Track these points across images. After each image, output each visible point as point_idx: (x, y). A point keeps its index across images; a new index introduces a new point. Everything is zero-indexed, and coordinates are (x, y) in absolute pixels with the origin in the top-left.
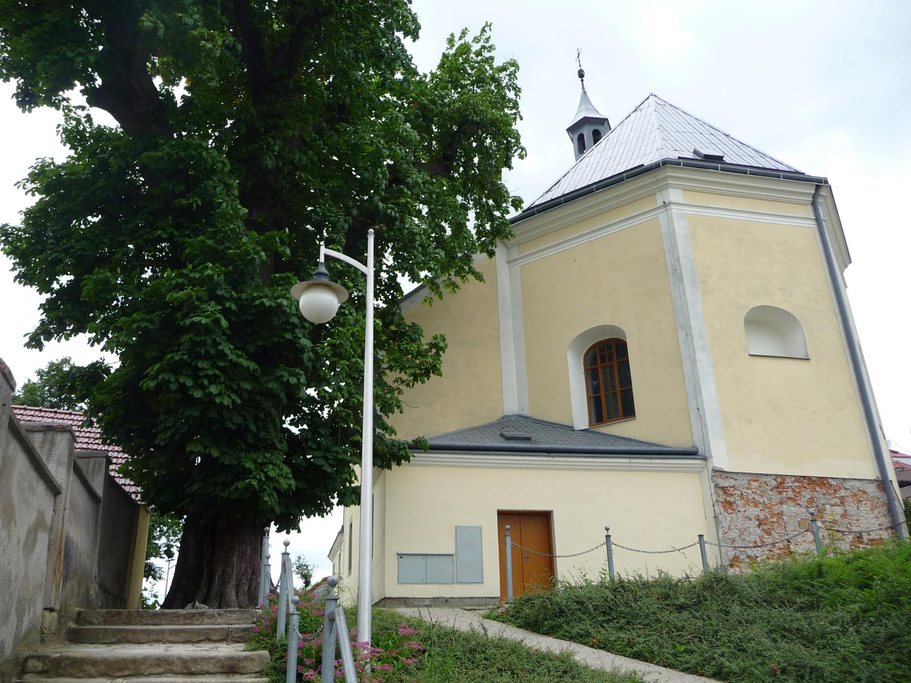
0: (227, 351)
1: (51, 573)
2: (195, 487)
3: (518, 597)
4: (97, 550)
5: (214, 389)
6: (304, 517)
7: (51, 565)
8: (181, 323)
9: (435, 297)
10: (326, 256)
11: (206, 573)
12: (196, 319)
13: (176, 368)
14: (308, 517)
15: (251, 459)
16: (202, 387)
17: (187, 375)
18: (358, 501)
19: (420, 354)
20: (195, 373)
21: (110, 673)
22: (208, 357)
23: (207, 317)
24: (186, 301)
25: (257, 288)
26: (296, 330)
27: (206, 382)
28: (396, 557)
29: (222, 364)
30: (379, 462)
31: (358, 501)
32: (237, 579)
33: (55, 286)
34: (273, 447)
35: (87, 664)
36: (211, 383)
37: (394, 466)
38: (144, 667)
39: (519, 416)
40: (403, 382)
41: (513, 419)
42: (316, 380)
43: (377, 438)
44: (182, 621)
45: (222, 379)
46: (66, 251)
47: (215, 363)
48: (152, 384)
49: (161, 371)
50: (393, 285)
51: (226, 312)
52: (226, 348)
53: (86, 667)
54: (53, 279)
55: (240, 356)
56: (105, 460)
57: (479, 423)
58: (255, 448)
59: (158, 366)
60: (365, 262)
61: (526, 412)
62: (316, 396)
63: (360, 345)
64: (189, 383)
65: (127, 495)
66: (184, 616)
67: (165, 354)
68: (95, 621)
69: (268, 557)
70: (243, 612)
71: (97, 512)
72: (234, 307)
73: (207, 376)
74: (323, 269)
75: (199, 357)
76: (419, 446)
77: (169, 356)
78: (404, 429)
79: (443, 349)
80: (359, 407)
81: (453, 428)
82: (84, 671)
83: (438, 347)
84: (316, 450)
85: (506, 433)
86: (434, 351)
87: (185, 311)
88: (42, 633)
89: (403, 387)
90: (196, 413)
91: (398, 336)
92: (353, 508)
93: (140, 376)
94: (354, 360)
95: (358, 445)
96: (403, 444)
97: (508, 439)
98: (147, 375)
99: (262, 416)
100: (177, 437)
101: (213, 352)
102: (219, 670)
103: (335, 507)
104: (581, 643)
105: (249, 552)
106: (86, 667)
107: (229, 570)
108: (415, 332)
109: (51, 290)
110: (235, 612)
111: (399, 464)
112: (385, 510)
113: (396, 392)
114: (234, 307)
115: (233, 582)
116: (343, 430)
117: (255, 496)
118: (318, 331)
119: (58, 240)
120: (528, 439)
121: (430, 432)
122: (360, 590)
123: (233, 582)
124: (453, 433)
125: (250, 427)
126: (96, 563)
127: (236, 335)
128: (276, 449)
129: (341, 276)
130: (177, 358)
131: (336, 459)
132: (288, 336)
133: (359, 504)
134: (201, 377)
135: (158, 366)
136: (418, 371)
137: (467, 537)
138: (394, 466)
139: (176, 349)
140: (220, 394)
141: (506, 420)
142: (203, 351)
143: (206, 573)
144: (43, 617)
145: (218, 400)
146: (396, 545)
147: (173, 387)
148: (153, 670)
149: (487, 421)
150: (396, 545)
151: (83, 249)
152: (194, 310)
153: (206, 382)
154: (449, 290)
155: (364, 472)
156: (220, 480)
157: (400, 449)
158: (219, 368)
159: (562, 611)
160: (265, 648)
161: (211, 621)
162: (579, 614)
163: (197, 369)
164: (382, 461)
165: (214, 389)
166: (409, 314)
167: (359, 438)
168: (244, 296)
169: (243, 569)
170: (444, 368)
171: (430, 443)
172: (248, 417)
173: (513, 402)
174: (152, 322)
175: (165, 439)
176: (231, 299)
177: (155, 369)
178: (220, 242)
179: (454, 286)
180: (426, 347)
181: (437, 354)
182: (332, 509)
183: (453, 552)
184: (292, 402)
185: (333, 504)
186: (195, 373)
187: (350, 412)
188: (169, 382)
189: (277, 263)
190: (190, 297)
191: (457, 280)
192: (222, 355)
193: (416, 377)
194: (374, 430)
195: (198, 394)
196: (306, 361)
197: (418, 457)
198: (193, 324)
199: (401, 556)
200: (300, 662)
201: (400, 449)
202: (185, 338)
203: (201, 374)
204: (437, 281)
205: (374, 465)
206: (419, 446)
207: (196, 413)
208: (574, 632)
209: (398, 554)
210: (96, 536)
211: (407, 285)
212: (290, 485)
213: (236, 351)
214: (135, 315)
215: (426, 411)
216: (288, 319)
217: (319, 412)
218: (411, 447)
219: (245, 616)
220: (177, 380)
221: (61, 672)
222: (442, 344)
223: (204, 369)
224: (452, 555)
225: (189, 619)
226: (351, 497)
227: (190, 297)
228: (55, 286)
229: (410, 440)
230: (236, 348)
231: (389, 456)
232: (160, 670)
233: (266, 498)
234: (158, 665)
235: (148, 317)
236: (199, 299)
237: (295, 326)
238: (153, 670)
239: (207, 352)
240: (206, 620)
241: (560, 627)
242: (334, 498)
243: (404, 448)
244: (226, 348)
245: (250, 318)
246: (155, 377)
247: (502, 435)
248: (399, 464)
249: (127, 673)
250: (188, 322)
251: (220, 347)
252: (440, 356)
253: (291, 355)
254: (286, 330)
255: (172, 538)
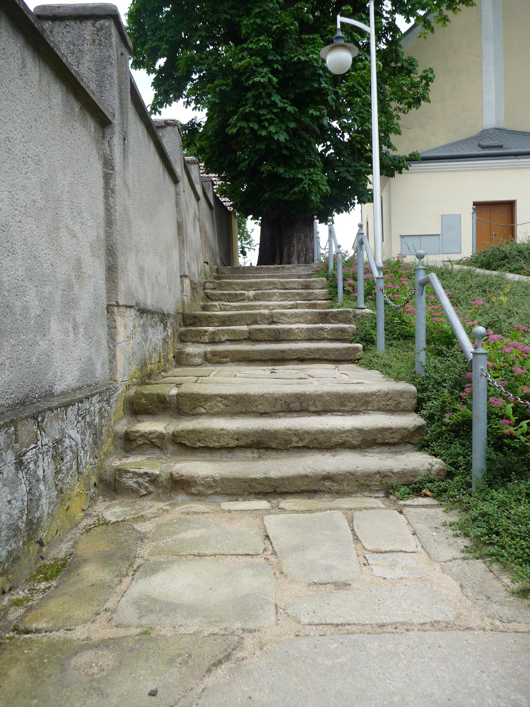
0: (277, 101)
1: (203, 244)
2: (267, 195)
3: (479, 251)
4: (216, 238)
5: (272, 129)
6: (335, 214)
7: (203, 239)
8: (247, 84)
9: (429, 32)
10: (342, 24)
11: (278, 251)
12: (257, 79)
13: (246, 117)
14: (339, 214)
15: (301, 173)
16: (264, 128)
17: (254, 121)
18: (371, 200)
19: (414, 85)
20: (259, 120)
21: (246, 289)
22: (265, 106)
23: (263, 77)
24: (247, 67)
25: (291, 50)
26: (321, 79)
27: (267, 124)
28: (400, 238)
29: (275, 111)
30: (385, 172)
31: (371, 200)
32: (297, 254)
33: (157, 67)
34: (315, 166)
35: (234, 284)
36: (270, 125)
37: (396, 173)
38: (262, 286)
39: (496, 129)
40: (400, 110)
41: (491, 132)
42: (336, 115)
43: (382, 155)
44: (272, 272)
45: (277, 121)
46: (161, 39)
47: (271, 110)
48: (234, 130)
49: (238, 120)
50: (393, 27)
51: (274, 72)
52: (276, 98)
53: (234, 286)
54: (155, 64)
55: (285, 103)
56: (211, 183)
57: (463, 137)
58: (301, 166)
59: (235, 117)
60: (367, 21)
61: (502, 125)
62: (338, 127)
63: (368, 84)
64: (256, 127)
65: (225, 208)
66: (273, 268)
67: (238, 108)
68: (226, 273)
69: (318, 233)
70: (306, 266)
71: (213, 216)
72: (280, 68)
73: (266, 120)
74: (340, 34)
75: (260, 107)
76: (414, 158)
77: (241, 109)
78: (402, 147)
79: (431, 80)
80: (368, 134)
81: (442, 143)
82: (233, 288)
83: (427, 79)
84: (341, 166)
85: (482, 143)
86: (424, 82)
87: (248, 75)
88: (206, 275)
89: (401, 114)
90: (263, 147)
91: (395, 72)
92: (368, 204)
93: (224, 125)
94: (364, 96)
95: (370, 160)
96: (402, 158)
97: (483, 147)
98: (229, 125)
99: (305, 144)
100: (252, 164)
101: (268, 102)
102: (300, 287)
103: (356, 205)
104: (517, 273)
105: (303, 237)
106: (234, 286)
107: (292, 249)
108: (407, 69)
109: (154, 71)
110: (301, 266)
111: (400, 172)
112: (391, 218)
113: (395, 118)
114: (280, 68)
115: (295, 256)
116: (359, 151)
117: (306, 195)
118: (337, 79)
119: (154, 32)
120: (501, 147)
121: (422, 149)
122: (376, 256)
123: (295, 256)
124: (440, 147)
125: (295, 155)
126: (217, 245)
127: (281, 89)
128: (317, 167)
129: (353, 35)
130: (247, 110)
131: (356, 171)
132: (316, 85)
133: (373, 202)
134: (263, 121)
135: (235, 117)
136: (411, 100)
137: (450, 222)
138: (396, 173)
139: (244, 103)
140: (277, 133)
141: (485, 133)
142: (262, 103)
143: (278, 251)
144: (204, 266)
145: (276, 137)
146: (399, 230)
147: (247, 131)
148: (267, 287)
149: (469, 136)
150: (399, 230)
151: (172, 37)
152: (253, 73)
153: (267, 124)
154: (440, 24)
155: (375, 180)
156: (282, 189)
157: (400, 162)
158: (274, 113)
159: (506, 257)
160: (323, 277)
161: (289, 271)
162: (518, 257)
163: (259, 116)
164: (387, 171)
165: (272, 129)
166: (407, 50)
167: (371, 154)
168: (285, 58)
169: (300, 247)
170: (431, 95)
171: (422, 155)
172: (297, 144)
173: (490, 118)
174: (227, 85)
175: (245, 167)
176: (277, 62)
177: (234, 119)
178: (263, 19)
179: (445, 19)
180: (418, 79)
181: (427, 84)
182: (354, 206)
183: (440, 233)
184: (324, 133)
185: (354, 203)
186: (259, 120)
187: (363, 136)
188: (244, 128)
189: (305, 27)
190: (250, 64)
191: (449, 13)
192: (274, 104)
193: (409, 105)
194: (379, 135)
195: (264, 133)
196: (330, 101)
197: (414, 166)
198: (254, 83)
199: (402, 237)
200: (344, 280)
201: (400, 162)
202: (249, 95)
203: (263, 118)
204: (428, 18)
205: (381, 174)
206: (414, 158)
207: (263, 147)
208: (512, 268)
209: (401, 236)
210: (214, 229)
211: (402, 24)
212: (327, 190)
213: (283, 100)
214: (216, 82)
215: (418, 131)
216: (315, 70)
217: (341, 139)
218: (408, 160)
219: (308, 268)
220: (249, 126)
221: (222, 288)
222: (430, 75)
223: (264, 115)
224: (439, 235)
225: (276, 270)
226: (366, 197)
227: (250, 64)
228: (157, 67)
229: (407, 155)
230: (282, 98)
231: (391, 167)
232: (270, 287)
233: (313, 198)
234: (269, 285)
235: (225, 82)
236: (255, 65)
237: (320, 75)
238: (267, 287)
239: (264, 102)
240: (286, 271)
241: (504, 265)
242: (354, 199)
243: (403, 160)
244: (276, 98)
245: (291, 75)
246: (235, 125)
247: (480, 146)
248: (400, 172)
249: (254, 289)
250: (250, 82)
251: (273, 99)
252: (429, 85)
253: (318, 97)
254: (314, 81)
255: (244, 242)
